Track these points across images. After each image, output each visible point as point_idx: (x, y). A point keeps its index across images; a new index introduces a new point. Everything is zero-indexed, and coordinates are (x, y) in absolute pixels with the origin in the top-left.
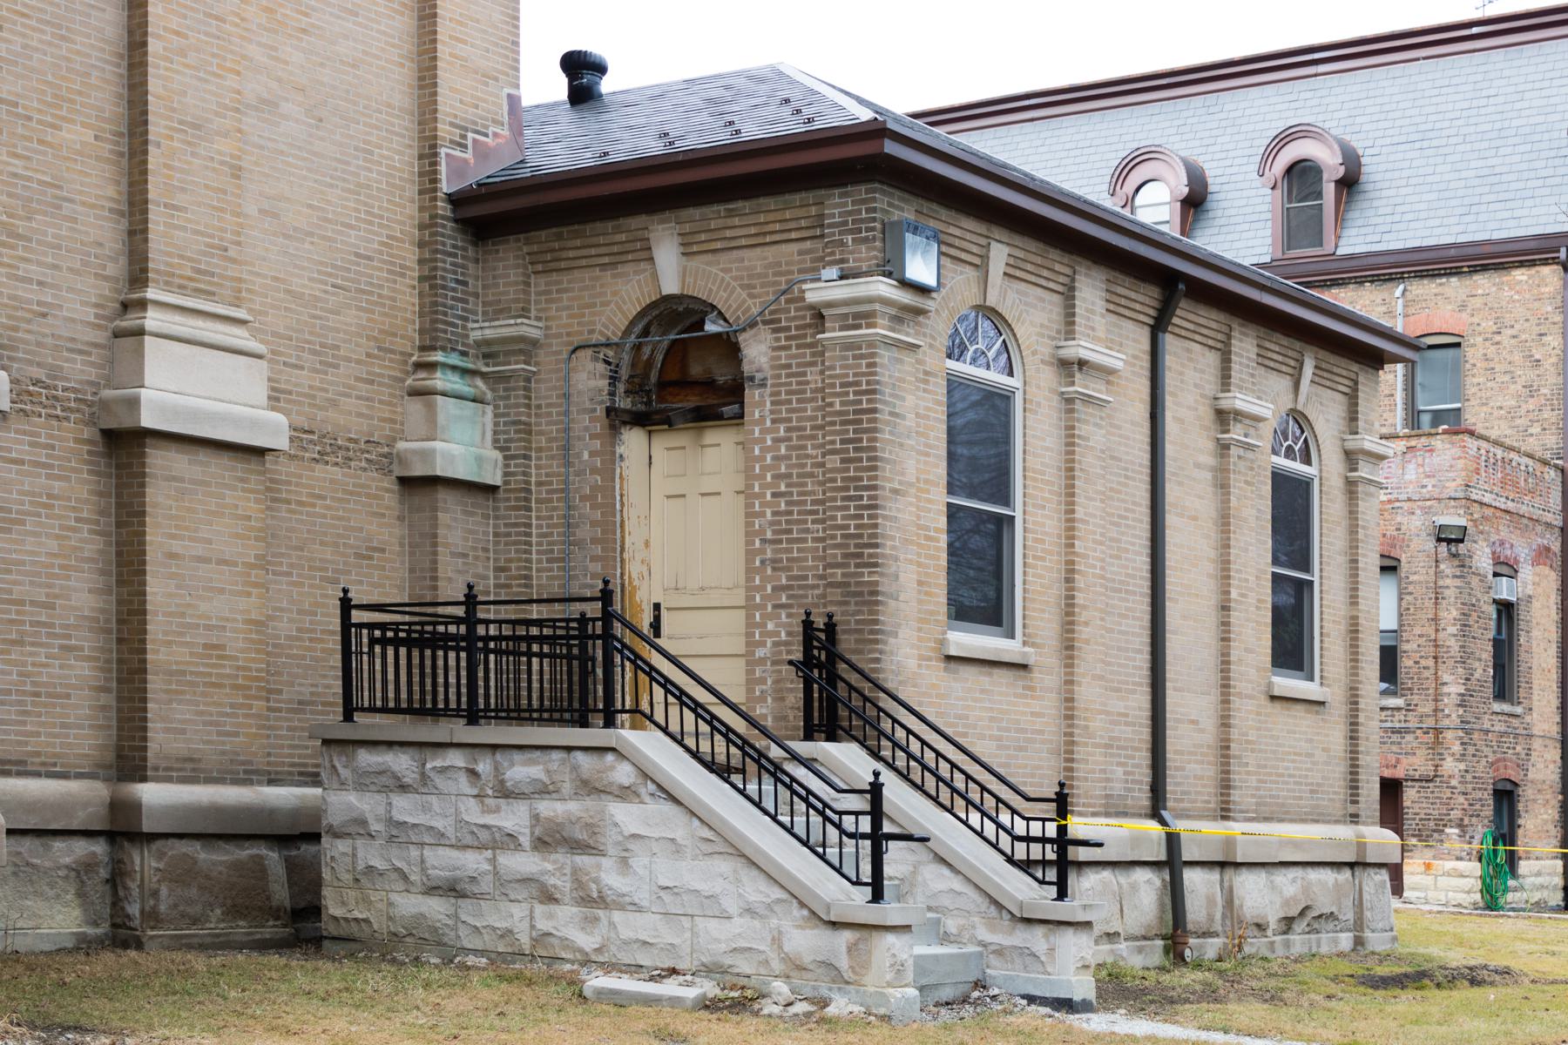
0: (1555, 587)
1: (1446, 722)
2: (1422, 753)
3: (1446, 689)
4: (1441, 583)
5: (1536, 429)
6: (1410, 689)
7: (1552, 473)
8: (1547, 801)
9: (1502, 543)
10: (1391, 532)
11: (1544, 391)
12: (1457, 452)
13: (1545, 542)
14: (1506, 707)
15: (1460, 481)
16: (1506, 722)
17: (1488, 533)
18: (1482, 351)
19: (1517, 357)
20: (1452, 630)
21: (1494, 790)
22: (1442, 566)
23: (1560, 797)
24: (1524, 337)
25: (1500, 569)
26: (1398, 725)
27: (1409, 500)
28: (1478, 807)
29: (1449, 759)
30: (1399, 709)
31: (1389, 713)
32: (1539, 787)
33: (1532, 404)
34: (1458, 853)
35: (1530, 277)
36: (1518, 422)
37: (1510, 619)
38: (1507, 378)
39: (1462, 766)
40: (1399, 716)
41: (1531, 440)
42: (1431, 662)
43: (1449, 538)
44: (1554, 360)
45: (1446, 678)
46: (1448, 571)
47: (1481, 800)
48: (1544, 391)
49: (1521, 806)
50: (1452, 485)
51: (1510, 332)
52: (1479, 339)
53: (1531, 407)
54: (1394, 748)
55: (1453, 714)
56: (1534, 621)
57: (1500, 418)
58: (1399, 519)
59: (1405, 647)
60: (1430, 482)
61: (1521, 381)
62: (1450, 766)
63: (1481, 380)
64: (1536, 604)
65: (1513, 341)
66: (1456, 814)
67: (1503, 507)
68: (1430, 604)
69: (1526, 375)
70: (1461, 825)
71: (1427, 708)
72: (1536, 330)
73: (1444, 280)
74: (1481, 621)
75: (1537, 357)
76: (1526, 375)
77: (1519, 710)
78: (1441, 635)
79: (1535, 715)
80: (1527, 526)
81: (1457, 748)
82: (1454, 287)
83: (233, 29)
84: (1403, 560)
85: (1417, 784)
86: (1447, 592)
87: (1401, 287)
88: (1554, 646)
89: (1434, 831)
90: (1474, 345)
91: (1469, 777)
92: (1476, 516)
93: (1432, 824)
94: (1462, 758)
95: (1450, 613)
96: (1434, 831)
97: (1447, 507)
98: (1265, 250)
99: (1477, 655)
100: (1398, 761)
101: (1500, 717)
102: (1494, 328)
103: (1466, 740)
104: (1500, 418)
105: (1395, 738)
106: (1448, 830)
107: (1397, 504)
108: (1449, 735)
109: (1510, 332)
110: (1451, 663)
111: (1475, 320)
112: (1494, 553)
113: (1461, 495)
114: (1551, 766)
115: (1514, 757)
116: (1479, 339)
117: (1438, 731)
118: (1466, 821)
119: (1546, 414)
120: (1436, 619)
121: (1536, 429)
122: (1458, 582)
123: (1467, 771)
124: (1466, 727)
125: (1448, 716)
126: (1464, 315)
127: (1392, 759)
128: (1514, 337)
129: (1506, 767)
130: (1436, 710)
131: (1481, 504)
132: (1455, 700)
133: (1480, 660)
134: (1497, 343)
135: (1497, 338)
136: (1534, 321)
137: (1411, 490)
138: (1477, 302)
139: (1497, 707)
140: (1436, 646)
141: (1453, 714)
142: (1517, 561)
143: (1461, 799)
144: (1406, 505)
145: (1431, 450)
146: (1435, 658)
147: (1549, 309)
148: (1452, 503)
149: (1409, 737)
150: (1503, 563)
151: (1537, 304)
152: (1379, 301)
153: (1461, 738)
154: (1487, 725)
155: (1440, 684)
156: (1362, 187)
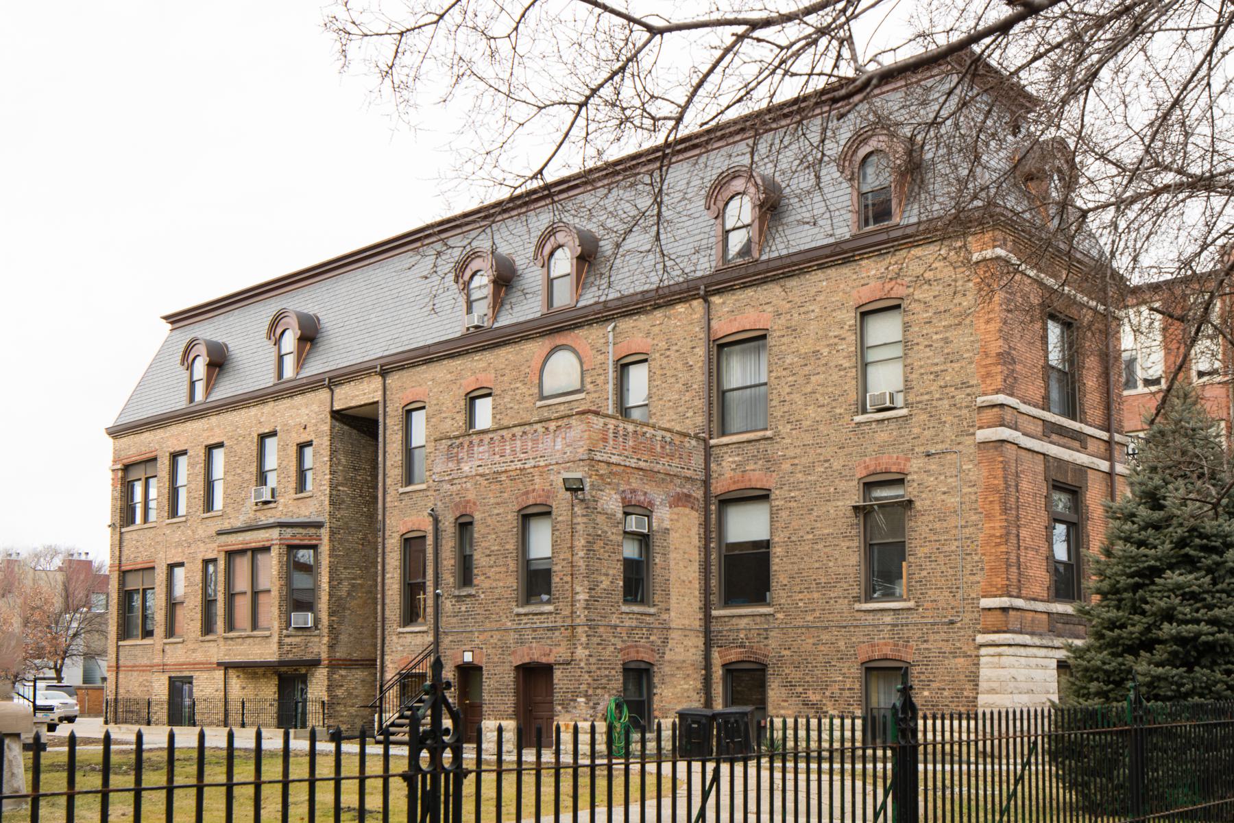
0: (697, 522)
1: (578, 621)
2: (564, 644)
3: (578, 597)
4: (575, 521)
5: (690, 414)
6: (558, 598)
7: (694, 442)
8: (688, 675)
9: (633, 491)
10: (548, 488)
11: (695, 386)
12: (584, 427)
13: (685, 491)
14: (636, 609)
15: (585, 448)
16: (637, 619)
17: (618, 484)
18: (659, 363)
19: (679, 365)
20: (581, 554)
21: (624, 669)
22: (576, 509)
23: (703, 672)
24: (683, 350)
25: (630, 510)
26: (550, 625)
27: (557, 463)
28: (604, 681)
29: (580, 648)
30: (551, 613)
31: (545, 616)
32: (679, 665)
33: (688, 396)
34: (584, 716)
35: (686, 309)
36: (680, 409)
37: (647, 546)
38: (673, 380)
39: (587, 652)
40: (552, 618)
41: (687, 421)
42: (568, 579)
43: (574, 488)
44: (700, 364)
45: (578, 589)
46: (579, 512)
47: (607, 676)
48: (695, 386)
49: (656, 680)
50: (581, 450)
51: (675, 348)
52: (657, 355)
53: (687, 399)
54: (549, 642)
55: (582, 615)
56: (672, 547)
57: (669, 408)
58: (552, 478)
59: (555, 568)
60: (568, 450)
61: (682, 381)
62: (581, 653)
63: (659, 383)
64: (673, 536)
65: (677, 354)
66: (583, 687)
67: (633, 465)
68: (568, 536)
69: (684, 376)
70: (586, 696)
71: (567, 612)
72: (690, 345)
73: (637, 317)
74: (607, 547)
75: (691, 363)
76: (684, 376)
77: (652, 610)
78: (575, 558)
79: (672, 614)
80: (663, 479)
81: (584, 639)
82: (643, 321)
83: (936, 361)
84: (554, 506)
85: (561, 667)
86: (579, 527)
87: (613, 325)
88: (697, 564)
89: (571, 700)
90: (654, 359)
91: (592, 660)
92: (601, 472)
93: (570, 695)
94: (587, 646)
95: (580, 542)
96: (571, 700)
97: (578, 466)
98: (538, 309)
99: (604, 571)
100: (551, 651)
101: (631, 616)
102: (666, 347)
103: (589, 633)
104: (669, 408)
105: (549, 634)
106: (579, 700)
107: (551, 467)
108: (580, 630)
109: (675, 348)
110: (580, 577)
111: (655, 342)
112: (623, 499)
113: (585, 457)
114: (693, 650)
115: (648, 645)
116: (657, 355)
117: (573, 627)
118: (590, 692)
119: (696, 402)
120: (572, 548)
121: (690, 414)
122: (585, 520)
123: (590, 656)
124: (592, 626)
125: (579, 616)
126: (649, 340)
127: (547, 649)
128: (677, 351)
129: (638, 652)
130: (572, 613)
131: (608, 463)
132: (583, 604)
133: (607, 575)
134: (668, 356)
135: (668, 353)
136: (689, 338)
137: (558, 457)
138: (656, 330)
139: (625, 608)
140: (572, 566)
141: (582, 615)
142: (651, 504)
143: (586, 676)
144: (555, 467)
145: (570, 428)
146: (572, 575)
147: (697, 329)
148: (582, 463)
149: (557, 633)
150: (635, 505)
151: (690, 327)
152: (601, 336)
153: (586, 632)
154: (614, 620)
155: (574, 593)
156: (598, 261)
